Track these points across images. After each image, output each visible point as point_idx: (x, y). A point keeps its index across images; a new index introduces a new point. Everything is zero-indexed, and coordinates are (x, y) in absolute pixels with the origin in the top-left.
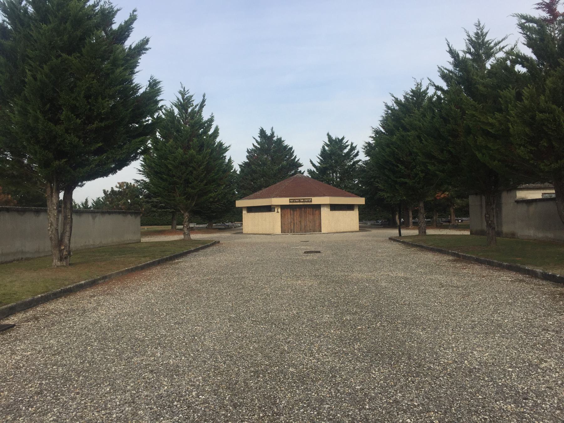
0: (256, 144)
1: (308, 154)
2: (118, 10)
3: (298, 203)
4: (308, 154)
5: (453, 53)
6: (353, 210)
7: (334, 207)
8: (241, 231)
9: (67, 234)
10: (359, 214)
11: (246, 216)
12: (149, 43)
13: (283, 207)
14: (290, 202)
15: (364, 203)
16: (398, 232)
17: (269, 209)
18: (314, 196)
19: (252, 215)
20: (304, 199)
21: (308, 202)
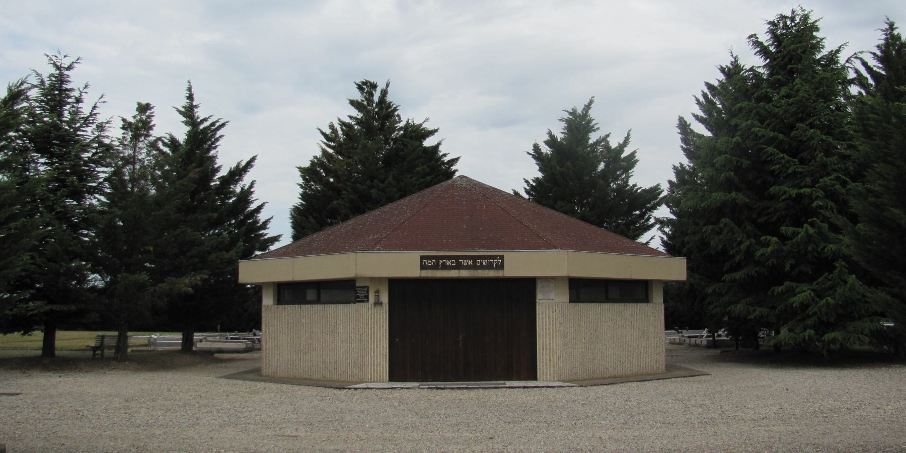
0: (206, 124)
1: (497, 158)
2: (588, 107)
3: (454, 274)
4: (497, 158)
7: (584, 290)
11: (275, 317)
13: (399, 288)
14: (423, 267)
15: (613, 147)
17: (345, 291)
20: (474, 258)
21: (490, 267)
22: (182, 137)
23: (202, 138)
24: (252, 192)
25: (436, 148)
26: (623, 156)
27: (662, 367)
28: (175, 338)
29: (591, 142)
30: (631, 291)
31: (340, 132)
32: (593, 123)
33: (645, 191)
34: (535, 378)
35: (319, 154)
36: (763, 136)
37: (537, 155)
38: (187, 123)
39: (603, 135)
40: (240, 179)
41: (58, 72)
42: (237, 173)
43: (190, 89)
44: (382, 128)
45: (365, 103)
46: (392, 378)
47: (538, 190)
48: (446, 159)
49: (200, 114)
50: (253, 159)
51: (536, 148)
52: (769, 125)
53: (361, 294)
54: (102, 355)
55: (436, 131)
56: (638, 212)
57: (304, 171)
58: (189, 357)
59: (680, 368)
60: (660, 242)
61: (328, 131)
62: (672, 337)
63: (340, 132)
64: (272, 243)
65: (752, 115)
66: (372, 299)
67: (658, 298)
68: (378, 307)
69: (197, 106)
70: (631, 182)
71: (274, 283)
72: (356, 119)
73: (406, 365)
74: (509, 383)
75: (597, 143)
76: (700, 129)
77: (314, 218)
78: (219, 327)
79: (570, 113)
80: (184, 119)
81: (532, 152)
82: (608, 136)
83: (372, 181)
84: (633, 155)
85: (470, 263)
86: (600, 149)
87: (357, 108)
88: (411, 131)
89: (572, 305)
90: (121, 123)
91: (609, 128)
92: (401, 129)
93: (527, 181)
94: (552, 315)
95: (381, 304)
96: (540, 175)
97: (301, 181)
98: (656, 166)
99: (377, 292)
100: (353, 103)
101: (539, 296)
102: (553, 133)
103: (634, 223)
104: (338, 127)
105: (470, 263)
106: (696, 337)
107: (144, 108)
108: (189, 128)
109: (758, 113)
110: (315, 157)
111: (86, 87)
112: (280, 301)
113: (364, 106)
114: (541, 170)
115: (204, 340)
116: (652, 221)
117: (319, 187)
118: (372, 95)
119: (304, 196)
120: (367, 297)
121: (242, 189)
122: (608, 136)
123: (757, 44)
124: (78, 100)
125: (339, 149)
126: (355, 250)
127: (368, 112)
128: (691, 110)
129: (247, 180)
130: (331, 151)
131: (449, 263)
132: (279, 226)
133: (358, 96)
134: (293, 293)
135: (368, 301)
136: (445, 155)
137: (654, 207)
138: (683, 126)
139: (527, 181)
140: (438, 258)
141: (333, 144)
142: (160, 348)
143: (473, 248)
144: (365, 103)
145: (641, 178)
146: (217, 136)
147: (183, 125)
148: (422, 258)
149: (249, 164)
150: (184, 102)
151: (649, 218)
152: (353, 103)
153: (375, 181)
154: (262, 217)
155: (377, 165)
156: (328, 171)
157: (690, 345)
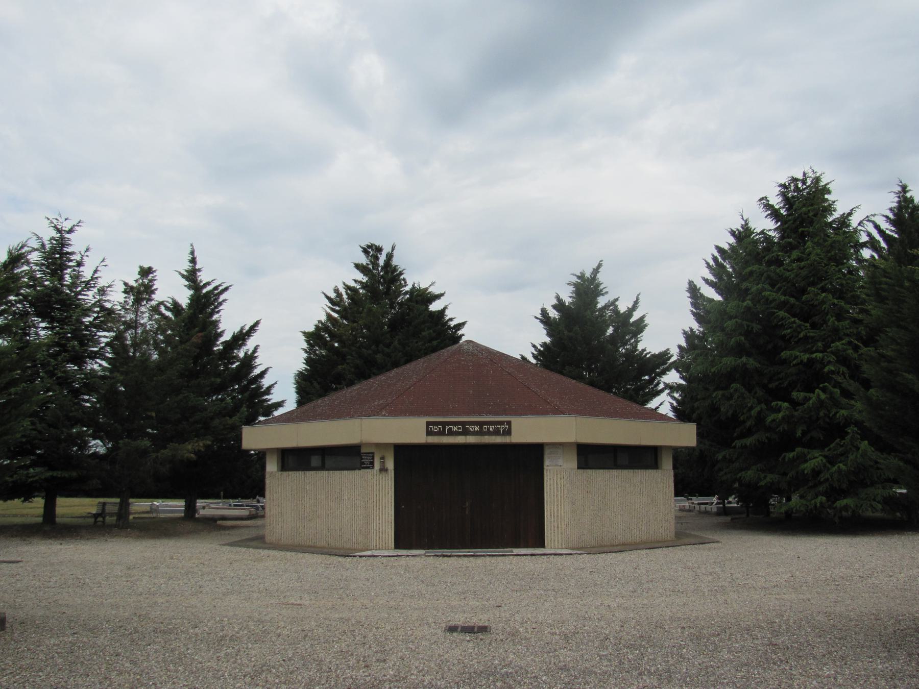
0: (209, 288)
1: (505, 323)
2: (596, 271)
3: (460, 440)
4: (505, 323)
7: (592, 456)
8: (261, 532)
9: (693, 541)
13: (405, 455)
14: (429, 433)
16: (59, 510)
17: (350, 457)
20: (481, 424)
21: (497, 433)
22: (184, 302)
23: (205, 302)
24: (256, 357)
26: (632, 320)
29: (599, 306)
30: (640, 457)
31: (345, 296)
32: (601, 287)
33: (654, 356)
34: (542, 545)
35: (324, 318)
36: (774, 300)
37: (545, 319)
38: (189, 287)
39: (612, 299)
41: (59, 235)
42: (241, 337)
43: (192, 253)
44: (387, 292)
45: (371, 267)
46: (398, 546)
48: (452, 324)
49: (203, 277)
50: (257, 324)
51: (544, 312)
52: (780, 288)
53: (366, 460)
55: (442, 295)
56: (647, 377)
57: (309, 336)
58: (192, 524)
60: (669, 407)
61: (333, 295)
62: (682, 504)
63: (345, 296)
64: (276, 409)
65: (763, 279)
66: (377, 465)
67: (667, 464)
69: (199, 270)
70: (640, 347)
71: (278, 449)
72: (361, 282)
74: (516, 551)
75: (606, 307)
76: (710, 293)
77: (319, 383)
79: (578, 277)
80: (187, 283)
81: (539, 316)
82: (617, 300)
83: (377, 346)
84: (642, 319)
85: (477, 428)
86: (609, 313)
87: (362, 272)
88: (417, 295)
90: (123, 287)
91: (618, 292)
92: (407, 293)
93: (534, 346)
94: (560, 482)
95: (386, 470)
96: (548, 340)
97: (305, 346)
98: (666, 331)
99: (383, 458)
101: (547, 462)
104: (343, 291)
105: (477, 428)
106: (706, 504)
107: (146, 272)
108: (192, 292)
109: (769, 277)
110: (320, 322)
111: (87, 250)
112: (284, 467)
113: (370, 270)
114: (549, 335)
115: (207, 507)
116: (661, 386)
117: (323, 352)
118: (377, 258)
119: (308, 361)
120: (372, 463)
121: (246, 353)
122: (617, 300)
123: (768, 206)
125: (344, 313)
128: (701, 274)
129: (250, 344)
130: (335, 315)
131: (455, 429)
132: (284, 392)
133: (363, 260)
134: (297, 459)
135: (373, 467)
136: (451, 319)
137: (664, 372)
138: (693, 290)
139: (534, 346)
140: (444, 424)
141: (337, 308)
142: (162, 515)
143: (480, 414)
144: (371, 267)
145: (650, 343)
146: (220, 300)
148: (428, 424)
149: (253, 328)
150: (187, 266)
151: (658, 384)
153: (381, 345)
154: (266, 382)
155: (383, 329)
156: (333, 336)
157: (700, 512)
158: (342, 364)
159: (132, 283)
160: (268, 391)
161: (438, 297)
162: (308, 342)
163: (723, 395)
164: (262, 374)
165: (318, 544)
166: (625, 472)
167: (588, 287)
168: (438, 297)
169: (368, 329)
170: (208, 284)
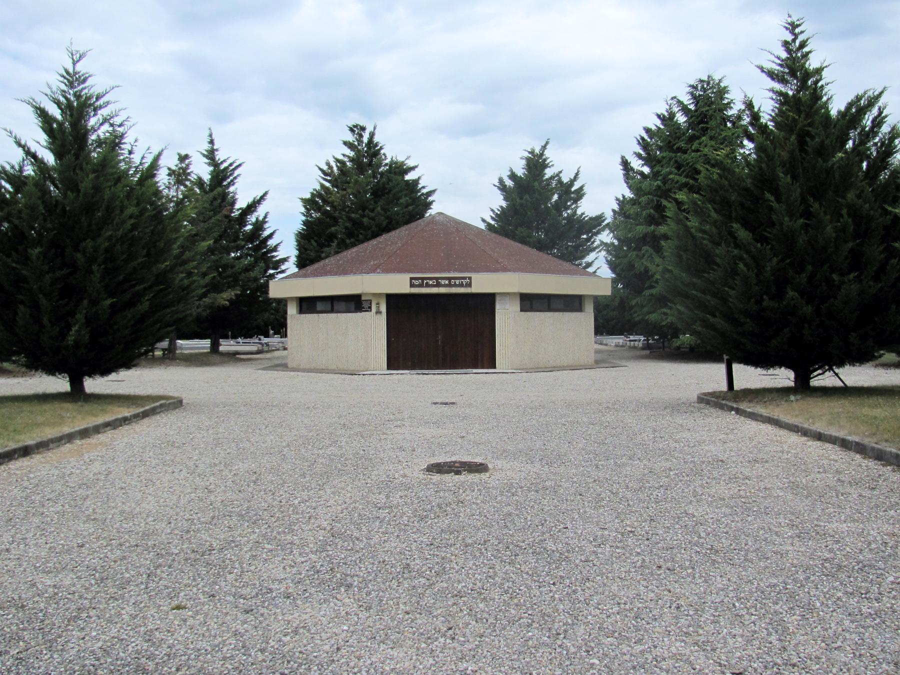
0: (225, 165)
1: (464, 191)
4: (464, 191)
5: (720, 81)
6: (580, 309)
7: (531, 302)
9: (126, 412)
10: (596, 320)
12: (650, 127)
13: (394, 301)
17: (355, 303)
18: (477, 270)
19: (310, 318)
20: (450, 279)
21: (461, 285)
22: (207, 178)
23: (222, 176)
24: (266, 222)
25: (416, 182)
26: (573, 189)
27: (590, 358)
28: (206, 343)
29: (547, 177)
30: (571, 303)
31: (335, 169)
32: (548, 161)
33: (591, 219)
34: (495, 367)
35: (318, 187)
36: (677, 182)
37: (502, 187)
38: (209, 164)
39: (556, 172)
40: (255, 211)
41: (111, 129)
42: (252, 207)
43: (211, 135)
44: (370, 164)
45: (356, 143)
46: (390, 367)
47: (503, 216)
48: (424, 191)
49: (220, 156)
50: (266, 194)
51: (501, 181)
52: (683, 171)
53: (365, 305)
54: (153, 355)
55: (416, 167)
56: (585, 236)
57: (305, 202)
58: (215, 356)
59: (610, 363)
60: (604, 261)
61: (325, 168)
62: (617, 341)
63: (335, 169)
64: (283, 264)
65: (672, 163)
67: (589, 309)
68: (379, 315)
69: (217, 150)
70: (579, 212)
71: (296, 298)
72: (348, 157)
73: (397, 359)
74: (475, 371)
75: (552, 178)
76: (637, 164)
77: (316, 241)
78: (230, 333)
79: (530, 153)
80: (207, 161)
81: (497, 184)
82: (561, 172)
83: (364, 211)
84: (581, 188)
85: (447, 282)
86: (554, 183)
87: (349, 148)
88: (396, 168)
89: (523, 313)
90: (167, 172)
91: (561, 163)
92: (386, 165)
93: (492, 210)
94: (508, 322)
95: (381, 313)
96: (504, 204)
97: (303, 210)
98: (603, 196)
99: (378, 304)
100: (345, 143)
102: (514, 170)
103: (581, 245)
104: (333, 164)
105: (447, 282)
106: (635, 341)
107: (183, 158)
108: (212, 168)
109: (676, 161)
110: (315, 190)
111: (136, 141)
112: (301, 311)
113: (356, 147)
114: (505, 199)
115: (227, 346)
116: (596, 244)
117: (318, 215)
118: (361, 136)
119: (305, 223)
120: (370, 308)
121: (257, 219)
122: (561, 172)
124: (130, 152)
125: (334, 182)
126: (361, 273)
127: (359, 151)
128: (631, 150)
129: (260, 212)
130: (328, 184)
131: (431, 282)
132: (287, 248)
133: (350, 138)
134: (308, 305)
136: (424, 187)
137: (598, 233)
138: (625, 164)
139: (492, 210)
140: (423, 279)
141: (329, 178)
142: (186, 352)
143: (449, 271)
144: (356, 143)
145: (587, 208)
146: (235, 175)
147: (206, 166)
148: (411, 279)
149: (262, 198)
150: (207, 146)
151: (594, 242)
152: (345, 143)
153: (367, 211)
154: (271, 243)
155: (367, 201)
156: (325, 201)
157: (630, 347)
158: (334, 226)
159: (174, 168)
160: (275, 249)
161: (413, 168)
162: (305, 207)
163: (637, 256)
164: (271, 236)
165: (330, 368)
166: (557, 314)
167: (538, 161)
168: (413, 168)
169: (355, 197)
170: (224, 161)
